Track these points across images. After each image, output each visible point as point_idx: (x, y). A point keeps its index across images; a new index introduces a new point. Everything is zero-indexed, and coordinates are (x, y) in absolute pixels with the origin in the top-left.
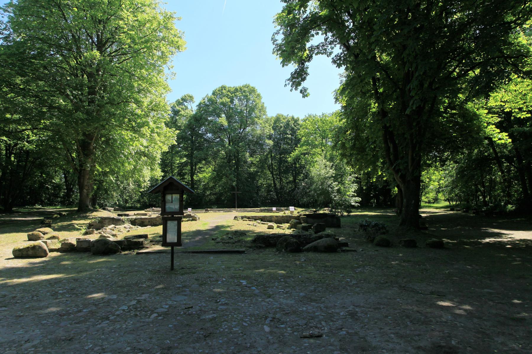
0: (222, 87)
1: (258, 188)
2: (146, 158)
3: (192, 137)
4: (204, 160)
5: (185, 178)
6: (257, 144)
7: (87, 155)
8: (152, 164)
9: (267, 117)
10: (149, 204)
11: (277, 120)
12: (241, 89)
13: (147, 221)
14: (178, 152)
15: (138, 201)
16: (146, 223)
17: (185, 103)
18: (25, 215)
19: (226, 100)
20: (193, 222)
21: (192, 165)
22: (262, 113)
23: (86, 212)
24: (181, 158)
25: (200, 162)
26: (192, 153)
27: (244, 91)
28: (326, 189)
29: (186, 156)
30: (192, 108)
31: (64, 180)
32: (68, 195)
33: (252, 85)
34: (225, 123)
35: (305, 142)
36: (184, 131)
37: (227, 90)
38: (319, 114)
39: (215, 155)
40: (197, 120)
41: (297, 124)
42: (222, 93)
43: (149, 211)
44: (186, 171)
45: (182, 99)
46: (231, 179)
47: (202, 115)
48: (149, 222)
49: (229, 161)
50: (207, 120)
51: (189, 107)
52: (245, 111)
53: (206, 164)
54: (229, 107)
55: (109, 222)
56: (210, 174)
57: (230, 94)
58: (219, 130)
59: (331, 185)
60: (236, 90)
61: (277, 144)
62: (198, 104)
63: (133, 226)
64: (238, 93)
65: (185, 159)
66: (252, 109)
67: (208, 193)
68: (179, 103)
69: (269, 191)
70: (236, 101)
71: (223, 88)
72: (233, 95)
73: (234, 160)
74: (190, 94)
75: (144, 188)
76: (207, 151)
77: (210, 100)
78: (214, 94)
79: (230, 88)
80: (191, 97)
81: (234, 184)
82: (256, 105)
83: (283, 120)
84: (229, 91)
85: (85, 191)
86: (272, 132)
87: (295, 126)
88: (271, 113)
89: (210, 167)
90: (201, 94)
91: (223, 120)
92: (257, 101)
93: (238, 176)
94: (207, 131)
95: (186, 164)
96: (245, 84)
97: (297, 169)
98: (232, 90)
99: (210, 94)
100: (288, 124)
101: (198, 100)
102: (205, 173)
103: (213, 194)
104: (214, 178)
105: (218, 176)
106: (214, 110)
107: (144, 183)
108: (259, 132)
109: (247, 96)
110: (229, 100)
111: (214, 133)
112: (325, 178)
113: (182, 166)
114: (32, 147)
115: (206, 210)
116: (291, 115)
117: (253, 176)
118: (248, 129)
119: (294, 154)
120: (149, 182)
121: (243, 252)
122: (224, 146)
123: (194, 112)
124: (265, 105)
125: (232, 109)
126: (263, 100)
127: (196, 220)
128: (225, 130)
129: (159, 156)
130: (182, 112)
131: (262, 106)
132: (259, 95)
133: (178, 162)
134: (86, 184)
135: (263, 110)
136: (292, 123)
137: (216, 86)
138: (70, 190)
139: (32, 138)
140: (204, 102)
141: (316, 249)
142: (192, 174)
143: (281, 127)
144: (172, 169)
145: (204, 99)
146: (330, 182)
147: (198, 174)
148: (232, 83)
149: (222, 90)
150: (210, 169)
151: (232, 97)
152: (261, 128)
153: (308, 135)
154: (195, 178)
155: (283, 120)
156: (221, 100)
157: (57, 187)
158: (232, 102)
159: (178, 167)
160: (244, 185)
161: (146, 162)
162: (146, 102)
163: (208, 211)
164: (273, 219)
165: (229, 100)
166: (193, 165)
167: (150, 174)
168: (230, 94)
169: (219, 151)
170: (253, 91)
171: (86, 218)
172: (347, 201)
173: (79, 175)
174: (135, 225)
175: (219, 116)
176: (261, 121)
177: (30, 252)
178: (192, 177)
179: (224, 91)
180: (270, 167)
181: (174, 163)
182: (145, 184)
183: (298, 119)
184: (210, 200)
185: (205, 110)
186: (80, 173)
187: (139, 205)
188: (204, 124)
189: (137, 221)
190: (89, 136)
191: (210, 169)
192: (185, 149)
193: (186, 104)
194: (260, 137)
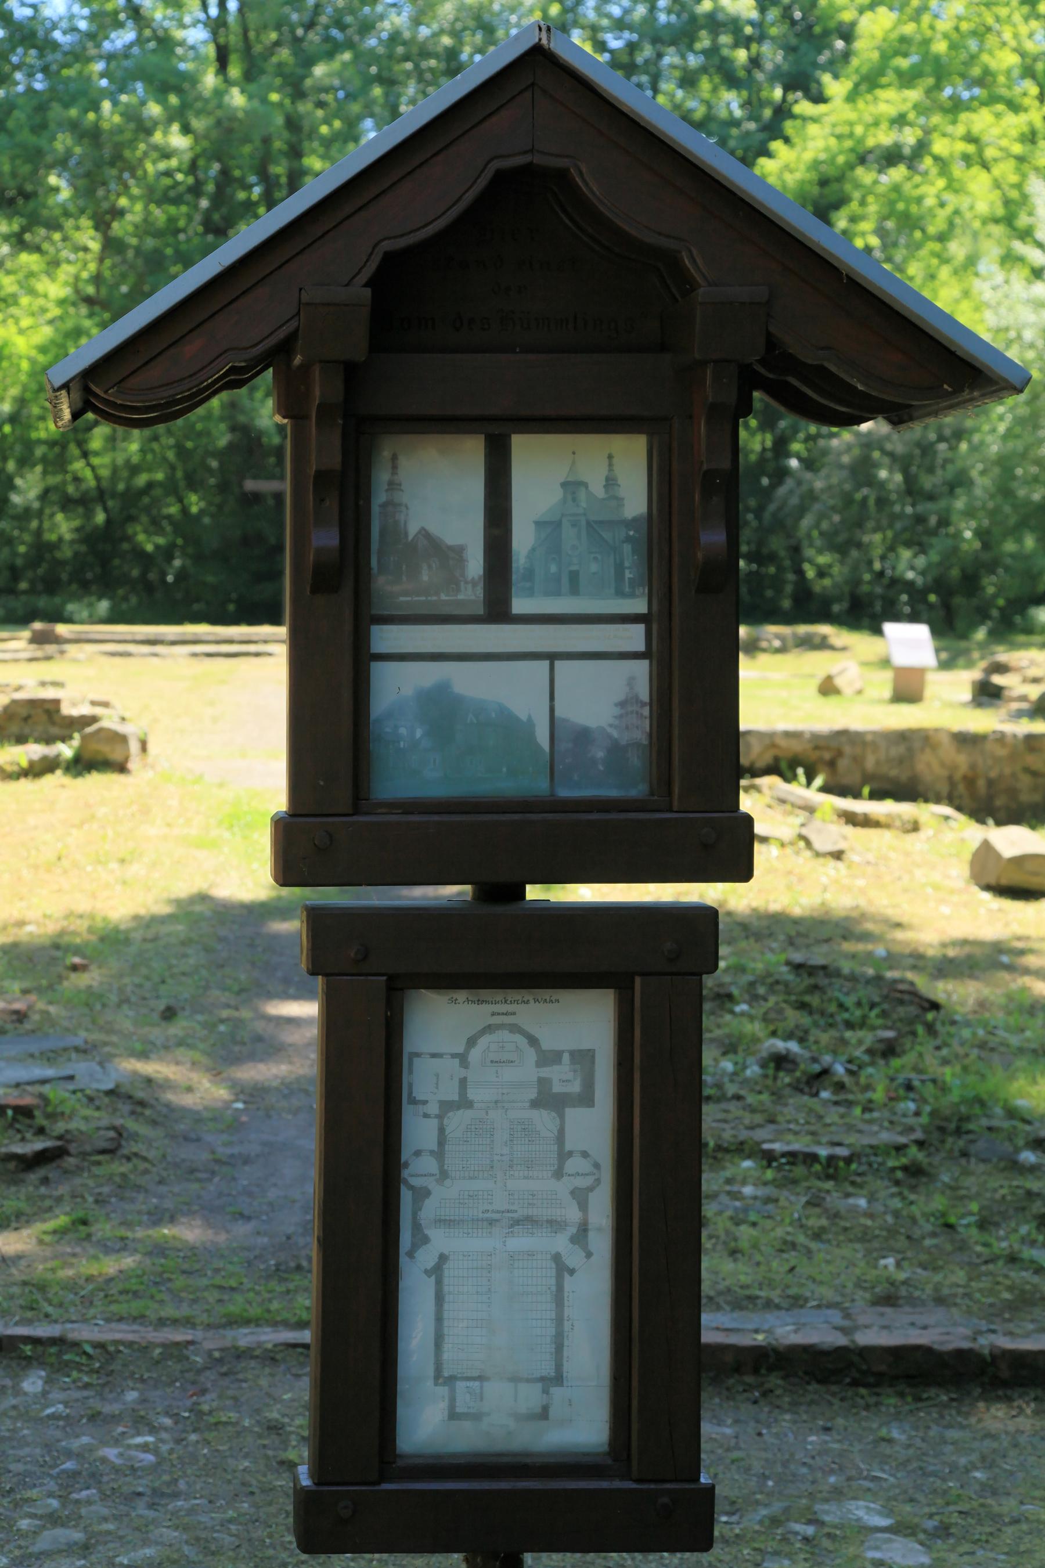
20: (95, 781)
39: (105, 161)
103: (67, 504)
122: (169, 83)
163: (58, 640)
164: (929, 767)
184: (42, 549)
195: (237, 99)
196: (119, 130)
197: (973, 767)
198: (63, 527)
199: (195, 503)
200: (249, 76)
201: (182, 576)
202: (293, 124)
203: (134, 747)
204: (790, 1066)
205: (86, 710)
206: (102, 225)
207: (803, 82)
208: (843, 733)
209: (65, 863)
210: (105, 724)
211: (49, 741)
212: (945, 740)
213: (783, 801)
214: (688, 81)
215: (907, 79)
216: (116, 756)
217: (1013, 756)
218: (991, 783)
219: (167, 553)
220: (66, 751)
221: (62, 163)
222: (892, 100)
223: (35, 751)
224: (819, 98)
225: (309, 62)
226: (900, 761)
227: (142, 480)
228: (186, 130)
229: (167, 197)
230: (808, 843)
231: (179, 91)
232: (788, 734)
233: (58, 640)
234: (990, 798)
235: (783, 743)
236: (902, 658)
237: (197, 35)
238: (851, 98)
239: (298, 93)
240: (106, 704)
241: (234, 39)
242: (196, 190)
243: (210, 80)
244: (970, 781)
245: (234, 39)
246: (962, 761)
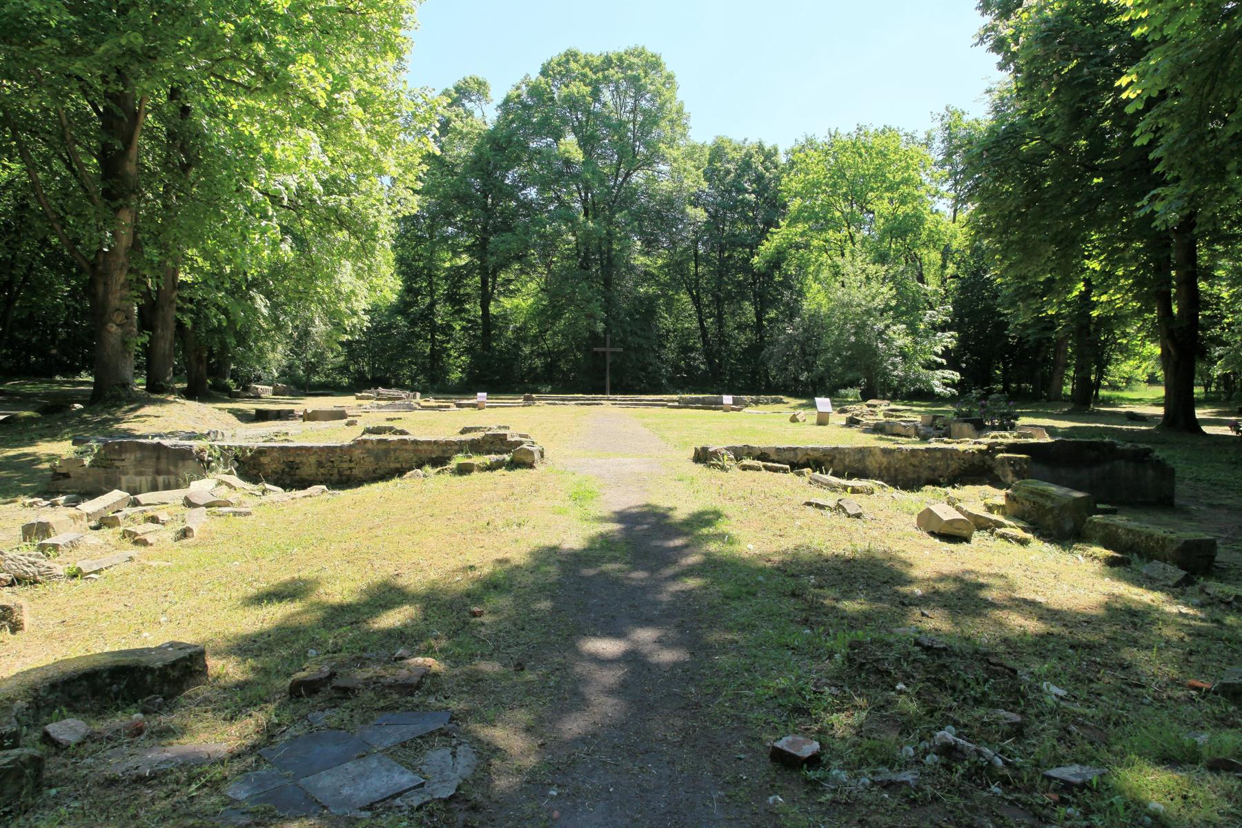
0: (566, 55)
1: (662, 339)
2: (345, 232)
3: (486, 197)
4: (519, 258)
5: (465, 311)
6: (659, 218)
8: (365, 251)
9: (691, 143)
10: (373, 378)
11: (718, 152)
12: (620, 59)
13: (313, 459)
15: (343, 370)
16: (306, 471)
17: (465, 101)
19: (579, 89)
20: (519, 472)
21: (488, 270)
22: (679, 130)
24: (456, 254)
25: (504, 265)
26: (485, 241)
27: (630, 67)
28: (869, 345)
29: (468, 249)
30: (486, 115)
33: (650, 50)
34: (578, 155)
35: (800, 211)
36: (463, 178)
37: (582, 62)
38: (846, 128)
39: (549, 244)
40: (500, 147)
41: (772, 163)
42: (568, 71)
43: (368, 398)
44: (469, 290)
46: (590, 316)
47: (513, 133)
48: (320, 464)
49: (585, 266)
51: (478, 113)
52: (631, 126)
53: (522, 271)
54: (588, 113)
55: (140, 462)
56: (531, 301)
57: (590, 73)
58: (563, 172)
59: (883, 332)
60: (608, 62)
61: (715, 219)
62: (500, 102)
63: (249, 486)
64: (611, 71)
65: (464, 260)
66: (652, 119)
67: (527, 350)
69: (685, 350)
70: (606, 95)
71: (571, 56)
72: (600, 75)
73: (598, 260)
75: (352, 333)
76: (526, 234)
77: (535, 91)
78: (544, 73)
79: (592, 56)
80: (481, 84)
81: (600, 327)
82: (663, 105)
83: (734, 154)
84: (587, 64)
86: (705, 185)
87: (767, 169)
88: (702, 132)
89: (532, 279)
90: (508, 73)
91: (570, 145)
92: (667, 95)
93: (609, 305)
96: (632, 46)
97: (772, 287)
98: (597, 62)
99: (535, 75)
100: (746, 165)
101: (498, 94)
102: (519, 299)
103: (538, 356)
104: (543, 312)
106: (545, 121)
107: (349, 317)
108: (665, 185)
109: (636, 79)
110: (589, 89)
111: (544, 185)
112: (868, 312)
113: (457, 276)
115: (526, 399)
116: (753, 140)
117: (646, 310)
118: (638, 178)
119: (768, 247)
120: (367, 317)
122: (570, 219)
123: (490, 127)
124: (686, 110)
125: (597, 115)
126: (680, 95)
127: (531, 466)
128: (576, 177)
129: (386, 228)
130: (458, 124)
131: (679, 112)
132: (670, 77)
133: (447, 265)
135: (679, 119)
136: (757, 161)
137: (554, 51)
140: (519, 96)
142: (486, 300)
143: (728, 172)
144: (430, 283)
145: (518, 88)
146: (881, 326)
147: (502, 299)
148: (596, 44)
149: (568, 61)
150: (532, 286)
151: (597, 81)
152: (672, 175)
153: (810, 190)
154: (493, 309)
155: (734, 154)
156: (565, 91)
158: (596, 94)
159: (446, 278)
160: (625, 331)
161: (346, 245)
163: (533, 399)
164: (871, 463)
165: (589, 89)
166: (488, 273)
167: (366, 286)
168: (590, 73)
169: (558, 233)
170: (654, 64)
172: (923, 382)
174: (255, 480)
175: (558, 136)
176: (675, 153)
178: (485, 307)
179: (573, 65)
180: (693, 287)
181: (438, 270)
182: (355, 320)
183: (776, 150)
184: (532, 369)
185: (520, 118)
187: (345, 381)
188: (518, 160)
189: (265, 460)
191: (532, 286)
192: (468, 228)
193: (469, 105)
194: (669, 202)
195: (590, 224)
196: (551, 234)
197: (889, 463)
198: (538, 362)
199: (579, 355)
200: (595, 217)
201: (574, 377)
202: (609, 233)
203: (537, 456)
204: (959, 755)
205: (518, 439)
206: (548, 266)
207: (770, 223)
208: (836, 448)
209: (490, 527)
210: (525, 446)
211: (500, 453)
212: (878, 452)
213: (817, 481)
214: (733, 223)
215: (806, 220)
216: (529, 460)
217: (906, 459)
218: (896, 470)
219: (570, 371)
220: (507, 457)
221: (534, 246)
222: (800, 227)
223: (494, 457)
224: (778, 226)
225: (614, 214)
226: (860, 461)
227: (562, 348)
228: (574, 235)
229: (568, 257)
230: (844, 510)
231: (571, 221)
232: (813, 449)
233: (533, 399)
234: (896, 476)
235: (811, 453)
236: (820, 409)
237: (577, 205)
238: (788, 226)
239: (610, 222)
240: (526, 436)
241: (589, 206)
242: (578, 254)
243: (582, 218)
244: (888, 469)
245: (589, 206)
246: (885, 460)
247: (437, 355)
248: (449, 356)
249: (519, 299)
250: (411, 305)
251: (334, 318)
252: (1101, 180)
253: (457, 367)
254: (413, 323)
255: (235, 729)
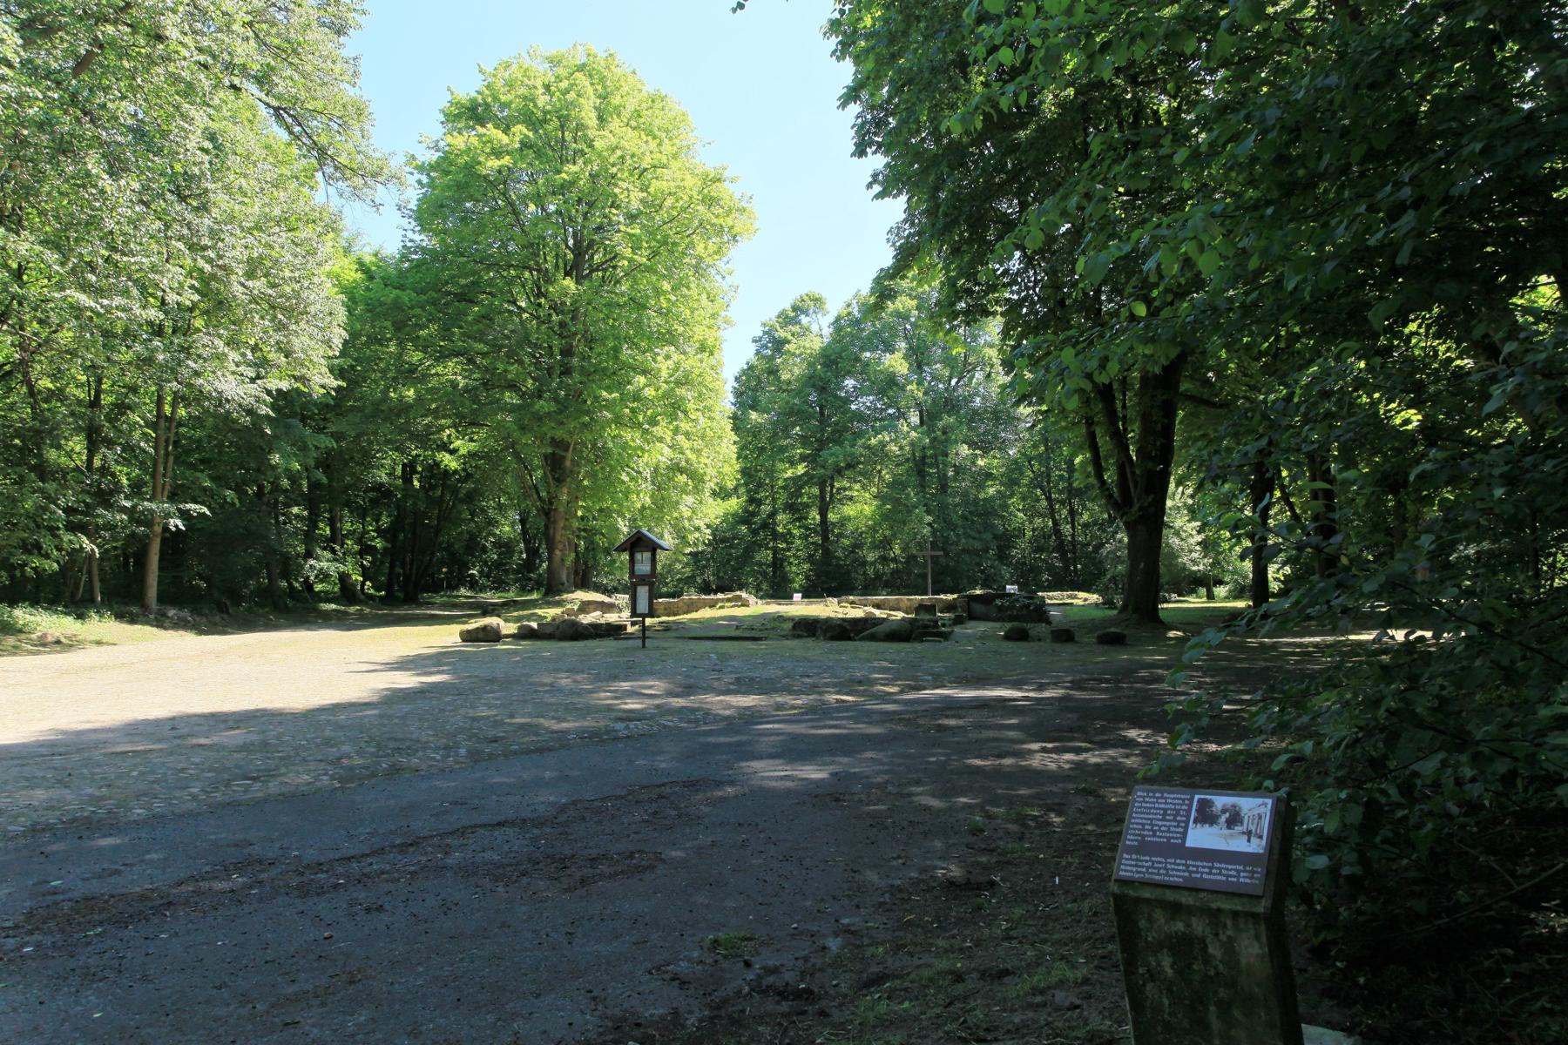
7: (559, 481)
14: (782, 450)
18: (444, 606)
21: (825, 483)
23: (560, 592)
29: (803, 458)
30: (819, 331)
31: (519, 527)
32: (529, 565)
40: (836, 360)
45: (795, 308)
50: (857, 359)
51: (814, 328)
62: (832, 319)
65: (801, 469)
68: (787, 319)
74: (816, 290)
85: (558, 552)
94: (859, 391)
95: (806, 479)
102: (859, 506)
105: (894, 510)
110: (915, 302)
114: (454, 465)
121: (760, 639)
134: (558, 538)
138: (533, 553)
139: (458, 449)
141: (873, 638)
154: (832, 517)
157: (505, 547)
162: (664, 368)
165: (915, 302)
167: (705, 514)
171: (559, 604)
173: (543, 523)
177: (481, 635)
178: (823, 514)
186: (547, 514)
190: (561, 445)
192: (804, 441)
247: (778, 563)
248: (790, 564)
249: (859, 506)
250: (753, 514)
251: (681, 534)
252: (1068, 226)
253: (798, 571)
254: (755, 532)
255: (737, 353)
